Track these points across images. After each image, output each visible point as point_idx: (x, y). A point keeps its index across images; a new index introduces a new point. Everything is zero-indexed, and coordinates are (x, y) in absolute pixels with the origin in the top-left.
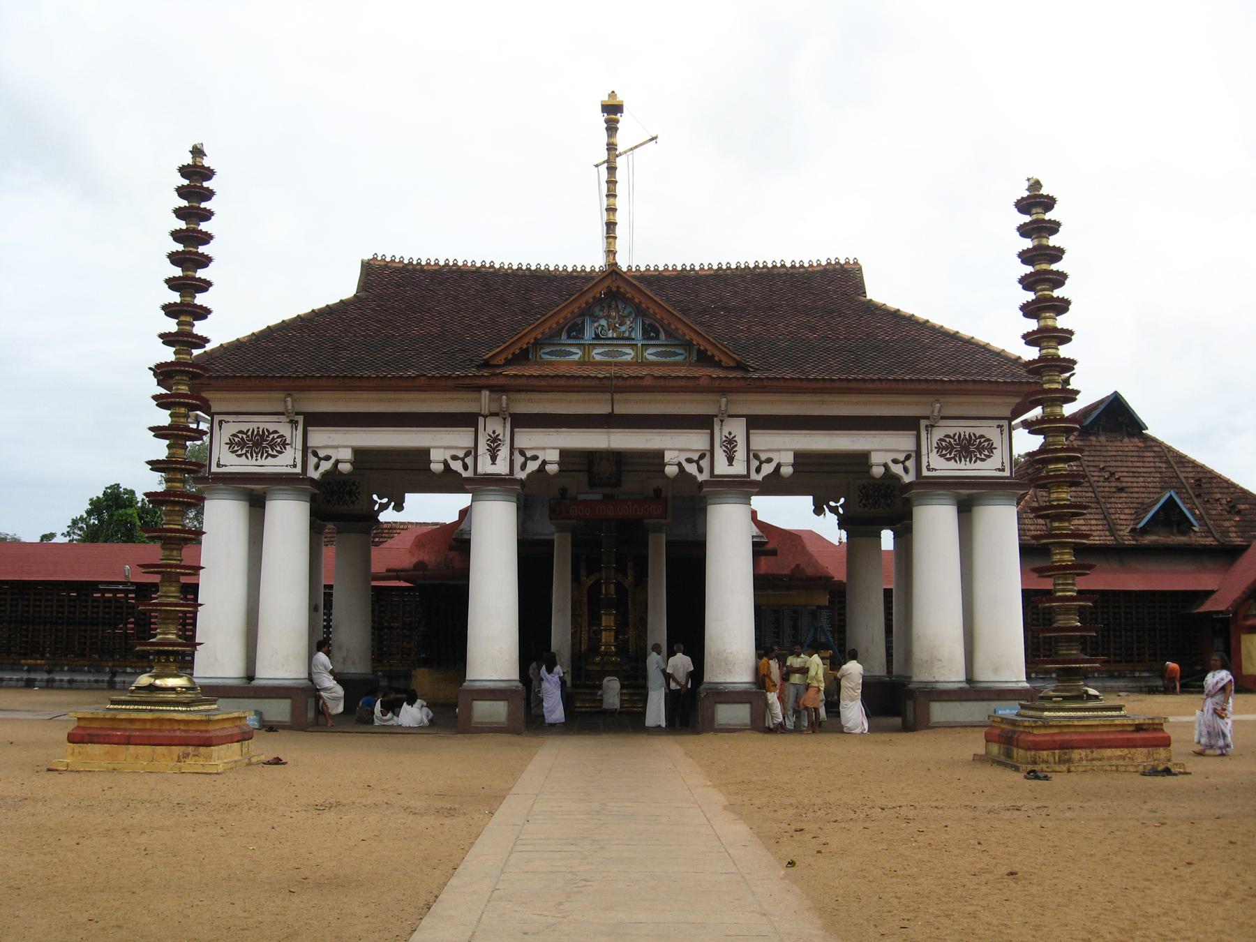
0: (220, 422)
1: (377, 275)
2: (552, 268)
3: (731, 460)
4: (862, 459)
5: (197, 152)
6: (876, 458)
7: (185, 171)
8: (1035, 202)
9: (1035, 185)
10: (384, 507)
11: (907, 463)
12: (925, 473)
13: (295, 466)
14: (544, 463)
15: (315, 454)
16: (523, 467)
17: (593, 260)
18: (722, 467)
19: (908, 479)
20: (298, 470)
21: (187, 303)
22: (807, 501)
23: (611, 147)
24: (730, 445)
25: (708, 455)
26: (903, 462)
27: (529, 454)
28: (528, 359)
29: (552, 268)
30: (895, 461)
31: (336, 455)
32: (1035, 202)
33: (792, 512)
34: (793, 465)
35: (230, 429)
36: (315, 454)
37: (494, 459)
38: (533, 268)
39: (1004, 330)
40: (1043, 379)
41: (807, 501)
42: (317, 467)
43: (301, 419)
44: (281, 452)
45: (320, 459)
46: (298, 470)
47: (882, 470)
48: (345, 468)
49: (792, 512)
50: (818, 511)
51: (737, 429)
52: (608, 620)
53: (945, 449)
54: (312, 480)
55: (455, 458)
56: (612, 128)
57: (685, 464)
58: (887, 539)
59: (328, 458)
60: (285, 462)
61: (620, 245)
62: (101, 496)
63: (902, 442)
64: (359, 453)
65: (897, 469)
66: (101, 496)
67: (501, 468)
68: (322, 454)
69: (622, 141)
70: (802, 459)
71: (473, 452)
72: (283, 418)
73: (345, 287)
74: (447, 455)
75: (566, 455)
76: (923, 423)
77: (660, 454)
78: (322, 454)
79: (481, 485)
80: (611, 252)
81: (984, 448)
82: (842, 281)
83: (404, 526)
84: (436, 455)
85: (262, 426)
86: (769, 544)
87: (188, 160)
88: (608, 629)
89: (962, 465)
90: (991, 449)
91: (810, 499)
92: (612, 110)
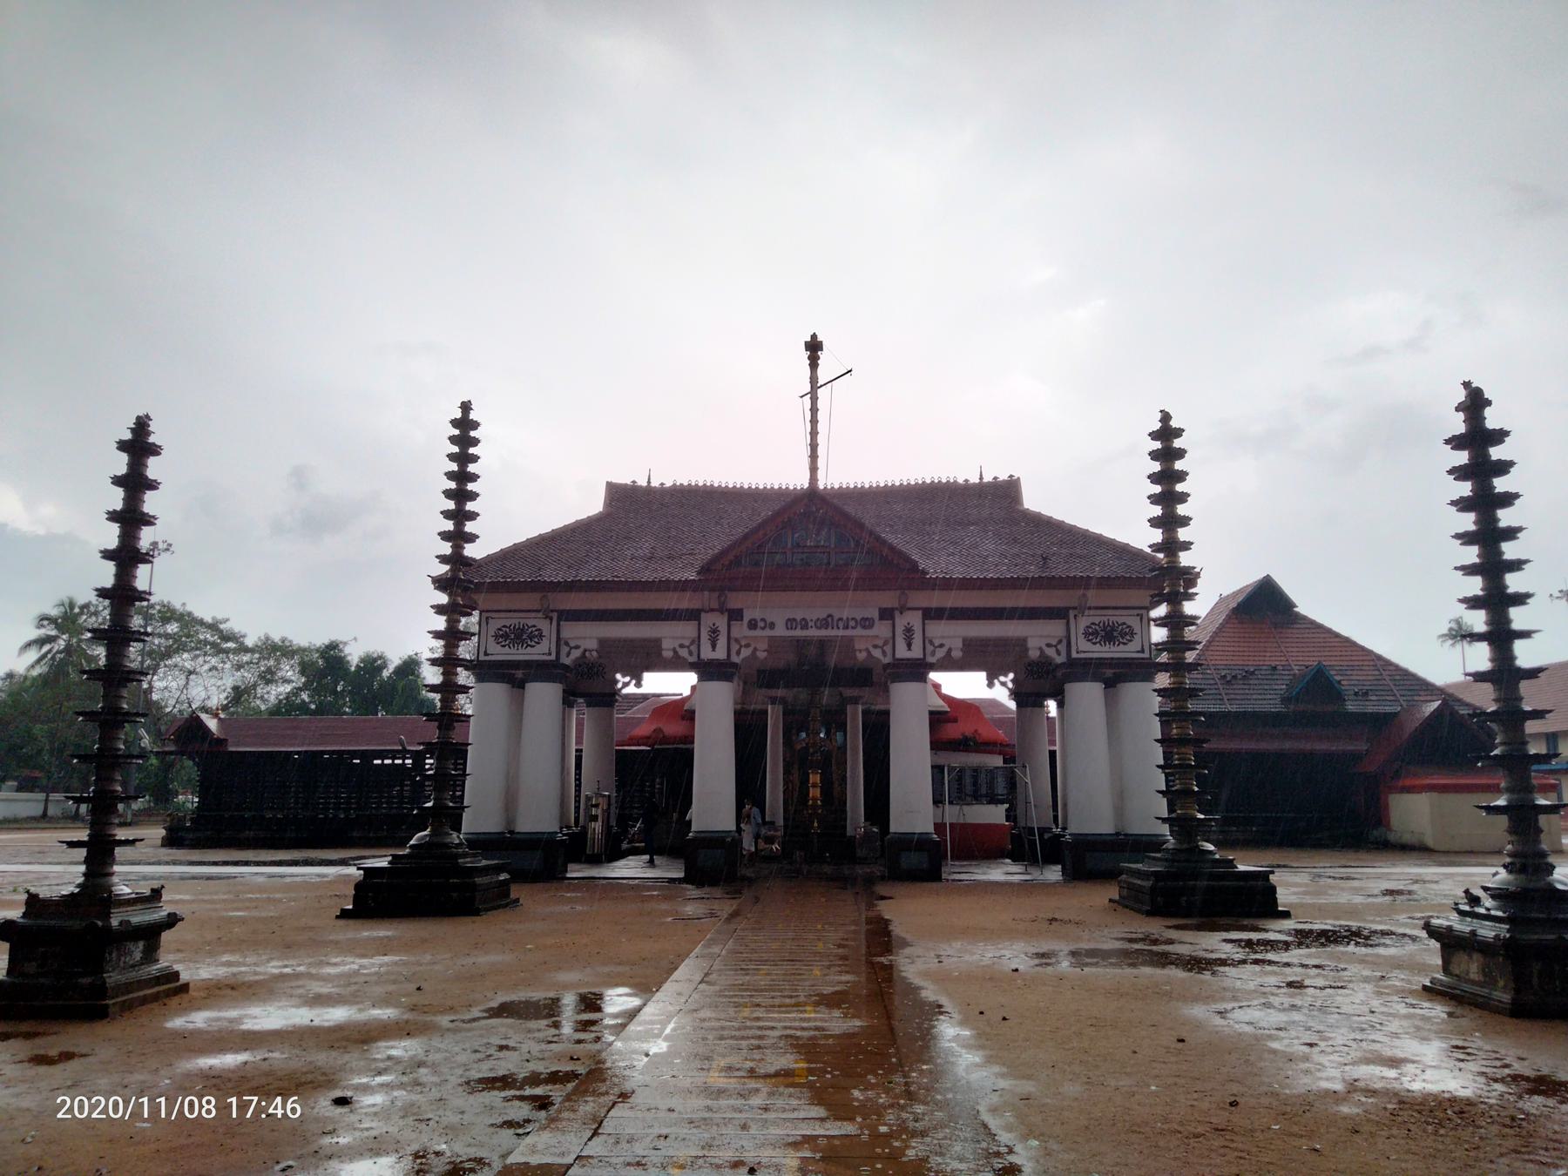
4: (1022, 643)
5: (1166, 417)
6: (1031, 643)
7: (455, 423)
8: (1166, 433)
9: (814, 336)
10: (626, 685)
12: (1074, 655)
14: (950, 650)
15: (567, 644)
16: (738, 653)
18: (902, 652)
19: (1060, 660)
20: (553, 657)
21: (458, 537)
22: (981, 676)
24: (714, 632)
28: (938, 878)
30: (1049, 645)
32: (1166, 433)
33: (964, 685)
35: (1084, 622)
37: (714, 647)
39: (1144, 537)
40: (1168, 577)
41: (981, 676)
42: (568, 654)
43: (555, 615)
46: (553, 657)
49: (964, 685)
50: (990, 685)
51: (915, 619)
52: (815, 778)
53: (1090, 634)
54: (566, 667)
55: (682, 646)
56: (814, 363)
58: (1052, 706)
59: (577, 647)
60: (539, 651)
61: (821, 475)
62: (151, 439)
63: (1054, 629)
65: (1051, 652)
66: (151, 439)
67: (720, 654)
68: (572, 644)
69: (823, 375)
71: (697, 641)
73: (593, 505)
75: (604, 643)
76: (1072, 614)
77: (1025, 640)
78: (572, 644)
80: (814, 469)
83: (645, 697)
84: (666, 644)
86: (950, 722)
87: (458, 415)
88: (814, 786)
89: (1107, 648)
90: (1132, 634)
91: (983, 675)
92: (814, 347)
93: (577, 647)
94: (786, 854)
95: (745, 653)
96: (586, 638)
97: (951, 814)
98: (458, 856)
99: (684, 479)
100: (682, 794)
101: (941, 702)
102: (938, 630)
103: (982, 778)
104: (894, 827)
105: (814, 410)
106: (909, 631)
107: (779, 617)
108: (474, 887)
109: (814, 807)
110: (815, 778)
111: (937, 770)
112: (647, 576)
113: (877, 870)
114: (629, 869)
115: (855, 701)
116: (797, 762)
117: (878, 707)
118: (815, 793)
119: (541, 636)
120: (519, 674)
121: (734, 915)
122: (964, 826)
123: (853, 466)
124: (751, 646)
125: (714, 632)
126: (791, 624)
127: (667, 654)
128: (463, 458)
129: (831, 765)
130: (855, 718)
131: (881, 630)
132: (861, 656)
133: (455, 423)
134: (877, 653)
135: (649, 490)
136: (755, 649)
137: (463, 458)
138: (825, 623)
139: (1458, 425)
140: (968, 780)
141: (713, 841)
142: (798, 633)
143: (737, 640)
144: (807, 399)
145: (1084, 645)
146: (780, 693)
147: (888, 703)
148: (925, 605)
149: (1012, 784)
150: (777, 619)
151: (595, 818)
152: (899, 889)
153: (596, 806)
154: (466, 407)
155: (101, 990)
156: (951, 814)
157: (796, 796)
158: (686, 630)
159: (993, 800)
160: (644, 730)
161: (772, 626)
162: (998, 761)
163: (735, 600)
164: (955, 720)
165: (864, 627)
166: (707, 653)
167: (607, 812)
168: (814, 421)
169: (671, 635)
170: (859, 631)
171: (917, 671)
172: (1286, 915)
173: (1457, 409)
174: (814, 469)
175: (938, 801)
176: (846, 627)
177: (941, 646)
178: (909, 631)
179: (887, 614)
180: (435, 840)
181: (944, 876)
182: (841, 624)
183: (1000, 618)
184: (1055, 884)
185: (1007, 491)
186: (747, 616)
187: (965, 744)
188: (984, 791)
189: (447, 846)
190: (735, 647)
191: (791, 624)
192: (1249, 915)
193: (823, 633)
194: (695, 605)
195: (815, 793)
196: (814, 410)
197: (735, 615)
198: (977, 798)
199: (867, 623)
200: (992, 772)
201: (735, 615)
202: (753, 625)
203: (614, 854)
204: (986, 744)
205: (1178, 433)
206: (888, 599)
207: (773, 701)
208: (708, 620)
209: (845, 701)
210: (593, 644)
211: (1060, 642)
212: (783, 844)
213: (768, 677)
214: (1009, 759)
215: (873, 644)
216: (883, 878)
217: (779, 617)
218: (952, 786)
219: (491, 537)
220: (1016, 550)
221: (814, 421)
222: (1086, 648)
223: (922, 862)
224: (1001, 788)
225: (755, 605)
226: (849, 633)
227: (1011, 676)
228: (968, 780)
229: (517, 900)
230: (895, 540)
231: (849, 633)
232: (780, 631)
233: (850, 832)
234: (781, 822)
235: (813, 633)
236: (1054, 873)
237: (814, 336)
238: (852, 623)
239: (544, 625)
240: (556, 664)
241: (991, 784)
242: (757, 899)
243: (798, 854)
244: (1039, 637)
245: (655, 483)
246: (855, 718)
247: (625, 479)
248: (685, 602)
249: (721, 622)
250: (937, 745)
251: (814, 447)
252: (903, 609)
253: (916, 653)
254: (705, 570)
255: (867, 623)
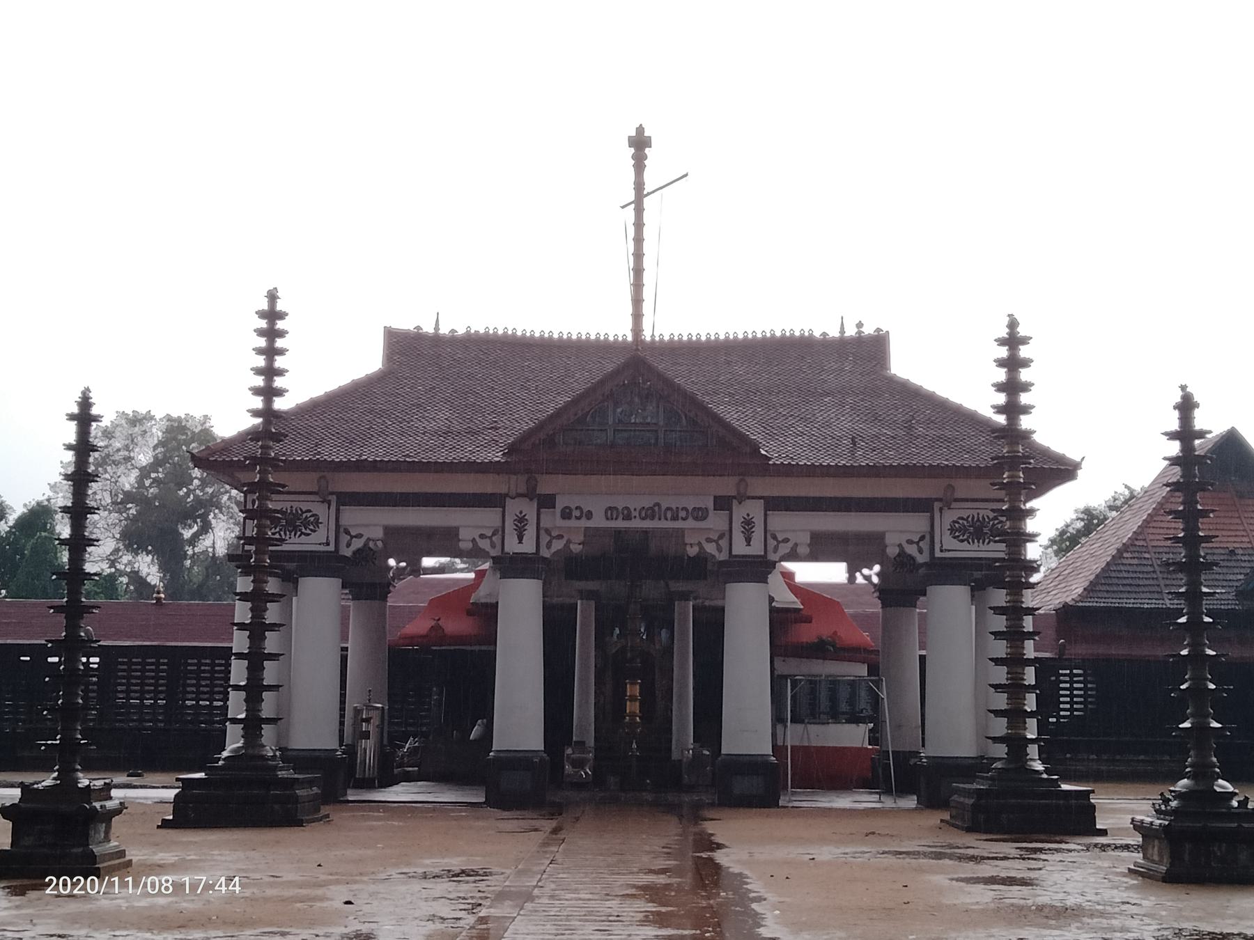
0: (941, 510)
1: (404, 347)
2: (703, 338)
3: (748, 541)
5: (1013, 324)
8: (1013, 340)
9: (640, 130)
11: (921, 544)
12: (938, 554)
13: (328, 544)
14: (796, 545)
15: (347, 532)
16: (549, 546)
17: (618, 328)
18: (740, 548)
20: (331, 548)
21: (269, 393)
23: (639, 186)
24: (521, 521)
25: (727, 536)
26: (490, 538)
27: (554, 534)
29: (611, 338)
31: (367, 533)
32: (1013, 340)
34: (809, 545)
35: (950, 516)
36: (775, 538)
38: (574, 337)
39: (982, 400)
42: (348, 545)
43: (333, 498)
44: (954, 522)
45: (352, 537)
47: (470, 545)
48: (576, 548)
51: (755, 510)
52: (633, 690)
53: (957, 530)
55: (482, 536)
57: (905, 545)
59: (359, 536)
60: (314, 541)
63: (915, 524)
64: (388, 530)
65: (911, 550)
67: (528, 547)
70: (388, 530)
72: (317, 498)
73: (368, 360)
74: (475, 534)
76: (937, 505)
79: (511, 566)
80: (637, 316)
81: (309, 523)
82: (869, 350)
84: (463, 534)
85: (295, 505)
86: (794, 627)
87: (264, 306)
88: (633, 698)
92: (640, 143)
93: (359, 536)
94: (598, 780)
95: (558, 545)
96: (369, 524)
97: (794, 735)
98: (276, 768)
99: (480, 326)
100: (484, 708)
101: (792, 598)
102: (782, 522)
103: (844, 693)
104: (729, 747)
105: (639, 225)
106: (748, 524)
107: (597, 506)
108: (296, 799)
109: (633, 724)
110: (633, 690)
111: (777, 682)
112: (442, 456)
113: (706, 798)
114: (399, 793)
115: (685, 596)
116: (613, 671)
117: (714, 603)
118: (633, 707)
119: (317, 523)
120: (291, 566)
121: (555, 831)
122: (806, 750)
123: (688, 311)
124: (568, 536)
125: (521, 521)
126: (611, 512)
127: (465, 545)
128: (271, 352)
129: (653, 672)
130: (686, 614)
131: (716, 521)
132: (692, 551)
133: (262, 314)
134: (710, 548)
135: (436, 341)
136: (569, 542)
137: (271, 352)
138: (650, 513)
139: (1004, 332)
140: (823, 695)
141: (517, 761)
142: (620, 524)
143: (548, 531)
144: (631, 210)
145: (950, 542)
146: (592, 585)
147: (724, 598)
148: (766, 494)
149: (876, 701)
150: (597, 505)
151: (366, 735)
152: (726, 813)
153: (368, 720)
154: (272, 297)
155: (93, 857)
156: (794, 735)
157: (609, 711)
158: (487, 518)
159: (855, 719)
160: (420, 626)
161: (589, 515)
162: (862, 670)
163: (546, 485)
164: (808, 620)
165: (696, 519)
166: (512, 546)
167: (381, 727)
168: (639, 240)
169: (472, 523)
170: (690, 523)
171: (759, 569)
172: (1103, 833)
173: (1175, 408)
174: (637, 316)
175: (778, 719)
176: (675, 518)
177: (786, 540)
178: (748, 524)
179: (723, 503)
180: (250, 751)
181: (781, 803)
182: (669, 515)
183: (848, 510)
184: (909, 810)
185: (869, 350)
186: (561, 503)
187: (821, 649)
188: (844, 707)
189: (263, 758)
190: (545, 539)
191: (611, 512)
192: (1056, 834)
193: (648, 524)
194: (503, 489)
195: (633, 707)
196: (639, 225)
197: (547, 502)
198: (835, 716)
199: (700, 514)
200: (853, 684)
201: (547, 502)
202: (566, 514)
203: (388, 780)
204: (844, 649)
205: (282, 316)
206: (725, 485)
207: (587, 595)
208: (514, 507)
209: (671, 598)
210: (379, 533)
211: (922, 538)
212: (594, 770)
213: (573, 567)
214: (873, 670)
215: (702, 537)
216: (712, 805)
217: (597, 506)
218: (796, 701)
219: (302, 386)
220: (875, 431)
221: (639, 240)
222: (952, 547)
223: (759, 787)
224: (863, 702)
225: (569, 490)
226: (679, 524)
227: (877, 568)
228: (823, 695)
229: (327, 816)
230: (731, 415)
231: (679, 524)
232: (599, 521)
233: (675, 755)
234: (591, 742)
235: (637, 524)
236: (910, 802)
237: (640, 130)
238: (682, 514)
239: (320, 510)
240: (335, 556)
241: (852, 701)
242: (577, 819)
243: (612, 780)
244: (900, 531)
245: (444, 330)
246: (686, 614)
247: (406, 323)
248: (488, 485)
249: (530, 510)
250: (779, 649)
251: (638, 271)
252: (742, 498)
253: (756, 549)
254: (512, 450)
255: (700, 514)
